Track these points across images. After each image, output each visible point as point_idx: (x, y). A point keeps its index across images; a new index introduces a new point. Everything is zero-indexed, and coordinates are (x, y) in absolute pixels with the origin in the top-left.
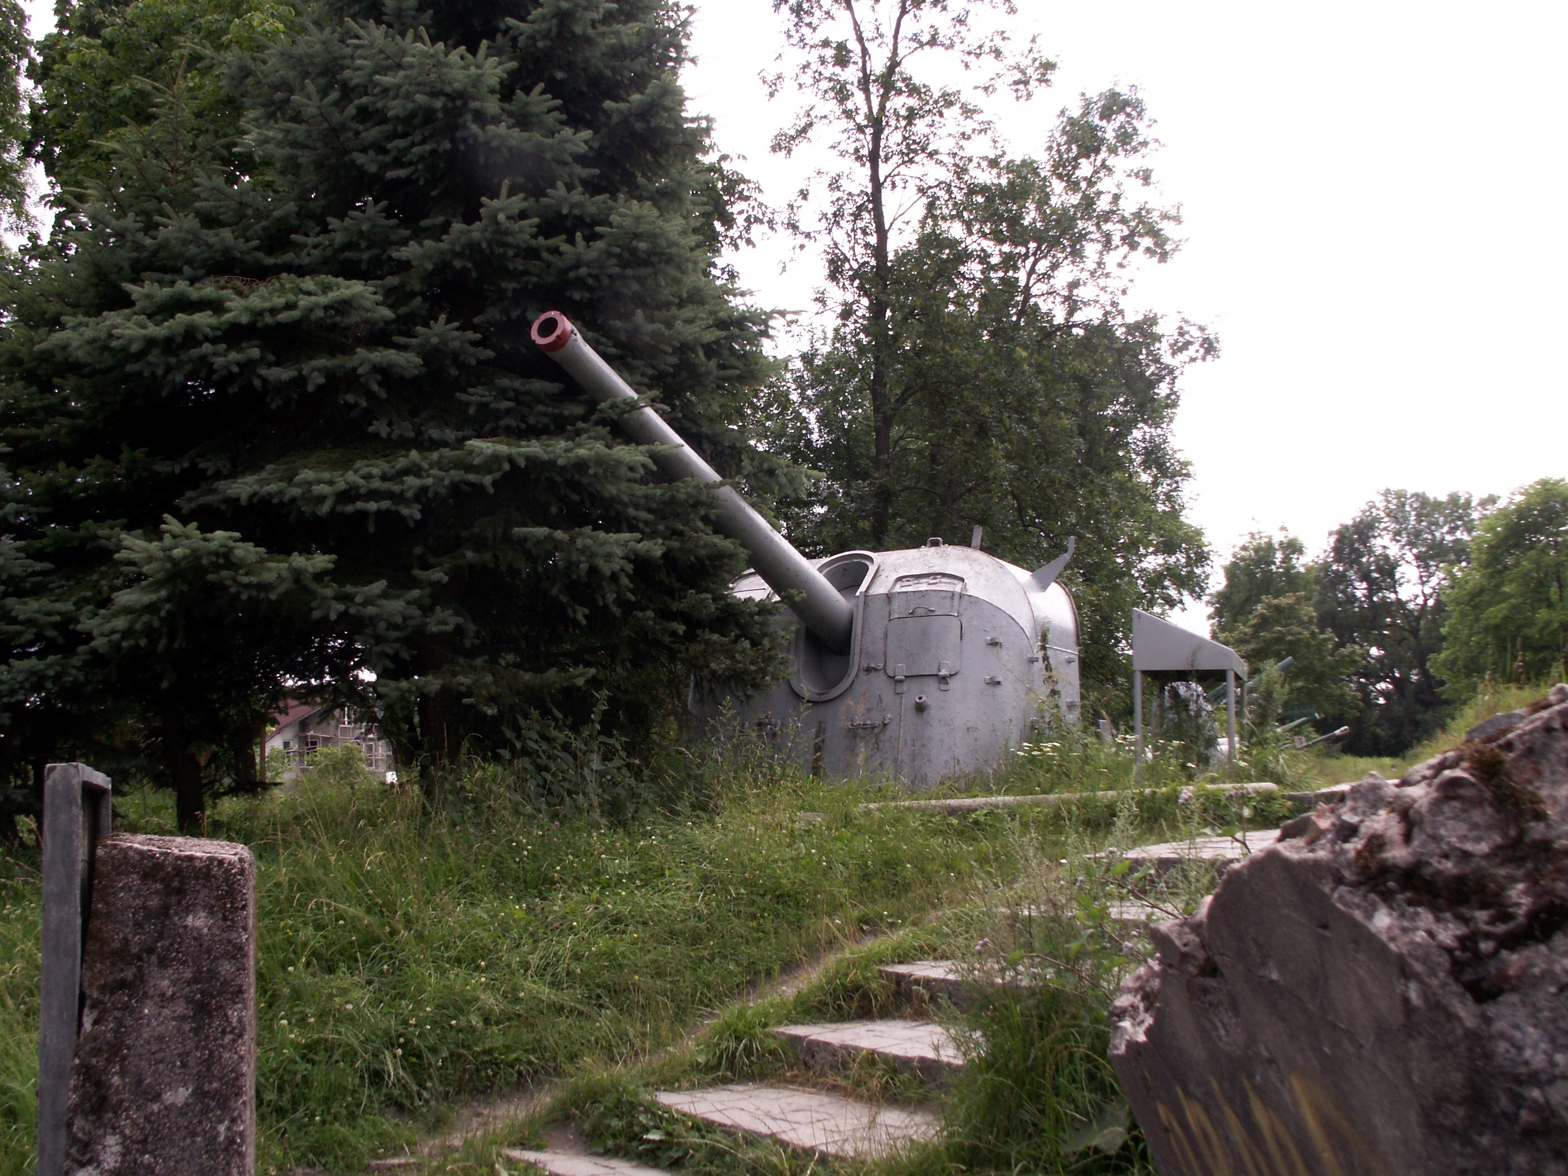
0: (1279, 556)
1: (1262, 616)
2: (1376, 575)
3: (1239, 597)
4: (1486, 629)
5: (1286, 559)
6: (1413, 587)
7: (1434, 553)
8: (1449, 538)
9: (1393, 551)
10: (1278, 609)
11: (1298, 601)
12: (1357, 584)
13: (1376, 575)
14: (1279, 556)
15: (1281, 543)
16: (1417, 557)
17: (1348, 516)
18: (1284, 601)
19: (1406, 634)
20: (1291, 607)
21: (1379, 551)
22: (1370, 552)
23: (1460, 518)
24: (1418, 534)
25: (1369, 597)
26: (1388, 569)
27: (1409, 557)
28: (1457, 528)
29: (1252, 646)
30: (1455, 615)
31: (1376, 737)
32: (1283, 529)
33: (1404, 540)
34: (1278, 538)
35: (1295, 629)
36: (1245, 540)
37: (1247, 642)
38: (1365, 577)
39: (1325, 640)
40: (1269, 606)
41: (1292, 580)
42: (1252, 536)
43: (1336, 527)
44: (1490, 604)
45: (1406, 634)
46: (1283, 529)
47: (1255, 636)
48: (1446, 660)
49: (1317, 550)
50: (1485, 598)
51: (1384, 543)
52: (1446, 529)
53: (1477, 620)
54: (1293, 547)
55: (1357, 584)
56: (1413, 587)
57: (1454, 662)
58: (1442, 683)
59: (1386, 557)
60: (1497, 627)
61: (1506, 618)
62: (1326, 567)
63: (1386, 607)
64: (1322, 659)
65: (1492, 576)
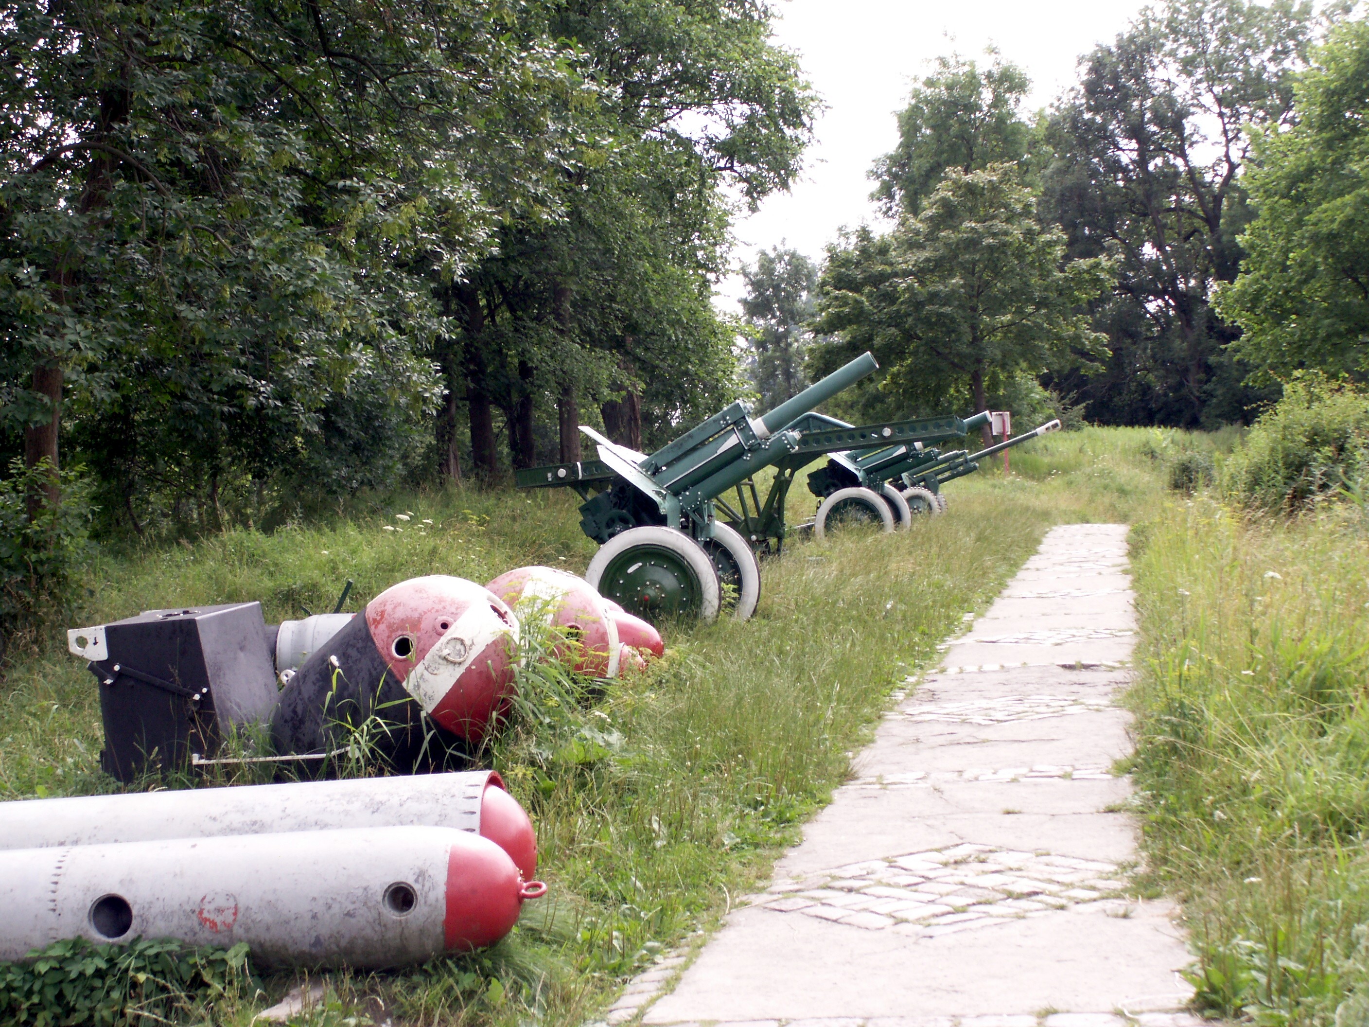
0: (987, 96)
1: (945, 203)
2: (1153, 128)
3: (920, 164)
4: (1316, 240)
5: (998, 101)
6: (1208, 145)
7: (1247, 94)
8: (1272, 68)
9: (1183, 90)
10: (971, 190)
11: (1006, 177)
12: (1123, 142)
13: (1153, 128)
14: (987, 96)
15: (989, 76)
16: (1220, 101)
17: (1109, 31)
18: (981, 177)
19: (1198, 223)
20: (994, 188)
21: (1161, 88)
22: (1145, 91)
23: (1292, 35)
24: (1222, 63)
25: (1142, 162)
26: (1173, 119)
27: (1208, 99)
28: (1286, 52)
29: (926, 254)
30: (1264, 212)
31: (1146, 389)
32: (993, 51)
33: (1199, 73)
34: (985, 65)
35: (999, 225)
36: (932, 70)
37: (921, 247)
38: (1136, 132)
39: (1050, 244)
40: (957, 185)
41: (1005, 135)
42: (944, 63)
43: (1089, 50)
44: (1325, 195)
45: (1198, 223)
46: (993, 51)
47: (931, 237)
48: (1244, 293)
49: (1051, 90)
50: (1318, 183)
51: (1164, 73)
52: (1268, 53)
53: (1299, 223)
54: (1010, 82)
55: (1123, 142)
56: (1208, 145)
57: (1256, 298)
58: (1234, 334)
59: (1171, 101)
60: (1332, 237)
61: (1350, 222)
62: (1073, 116)
63: (1168, 180)
64: (1045, 274)
65: (1329, 145)
